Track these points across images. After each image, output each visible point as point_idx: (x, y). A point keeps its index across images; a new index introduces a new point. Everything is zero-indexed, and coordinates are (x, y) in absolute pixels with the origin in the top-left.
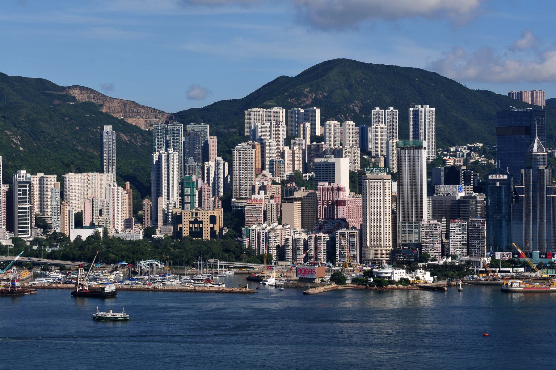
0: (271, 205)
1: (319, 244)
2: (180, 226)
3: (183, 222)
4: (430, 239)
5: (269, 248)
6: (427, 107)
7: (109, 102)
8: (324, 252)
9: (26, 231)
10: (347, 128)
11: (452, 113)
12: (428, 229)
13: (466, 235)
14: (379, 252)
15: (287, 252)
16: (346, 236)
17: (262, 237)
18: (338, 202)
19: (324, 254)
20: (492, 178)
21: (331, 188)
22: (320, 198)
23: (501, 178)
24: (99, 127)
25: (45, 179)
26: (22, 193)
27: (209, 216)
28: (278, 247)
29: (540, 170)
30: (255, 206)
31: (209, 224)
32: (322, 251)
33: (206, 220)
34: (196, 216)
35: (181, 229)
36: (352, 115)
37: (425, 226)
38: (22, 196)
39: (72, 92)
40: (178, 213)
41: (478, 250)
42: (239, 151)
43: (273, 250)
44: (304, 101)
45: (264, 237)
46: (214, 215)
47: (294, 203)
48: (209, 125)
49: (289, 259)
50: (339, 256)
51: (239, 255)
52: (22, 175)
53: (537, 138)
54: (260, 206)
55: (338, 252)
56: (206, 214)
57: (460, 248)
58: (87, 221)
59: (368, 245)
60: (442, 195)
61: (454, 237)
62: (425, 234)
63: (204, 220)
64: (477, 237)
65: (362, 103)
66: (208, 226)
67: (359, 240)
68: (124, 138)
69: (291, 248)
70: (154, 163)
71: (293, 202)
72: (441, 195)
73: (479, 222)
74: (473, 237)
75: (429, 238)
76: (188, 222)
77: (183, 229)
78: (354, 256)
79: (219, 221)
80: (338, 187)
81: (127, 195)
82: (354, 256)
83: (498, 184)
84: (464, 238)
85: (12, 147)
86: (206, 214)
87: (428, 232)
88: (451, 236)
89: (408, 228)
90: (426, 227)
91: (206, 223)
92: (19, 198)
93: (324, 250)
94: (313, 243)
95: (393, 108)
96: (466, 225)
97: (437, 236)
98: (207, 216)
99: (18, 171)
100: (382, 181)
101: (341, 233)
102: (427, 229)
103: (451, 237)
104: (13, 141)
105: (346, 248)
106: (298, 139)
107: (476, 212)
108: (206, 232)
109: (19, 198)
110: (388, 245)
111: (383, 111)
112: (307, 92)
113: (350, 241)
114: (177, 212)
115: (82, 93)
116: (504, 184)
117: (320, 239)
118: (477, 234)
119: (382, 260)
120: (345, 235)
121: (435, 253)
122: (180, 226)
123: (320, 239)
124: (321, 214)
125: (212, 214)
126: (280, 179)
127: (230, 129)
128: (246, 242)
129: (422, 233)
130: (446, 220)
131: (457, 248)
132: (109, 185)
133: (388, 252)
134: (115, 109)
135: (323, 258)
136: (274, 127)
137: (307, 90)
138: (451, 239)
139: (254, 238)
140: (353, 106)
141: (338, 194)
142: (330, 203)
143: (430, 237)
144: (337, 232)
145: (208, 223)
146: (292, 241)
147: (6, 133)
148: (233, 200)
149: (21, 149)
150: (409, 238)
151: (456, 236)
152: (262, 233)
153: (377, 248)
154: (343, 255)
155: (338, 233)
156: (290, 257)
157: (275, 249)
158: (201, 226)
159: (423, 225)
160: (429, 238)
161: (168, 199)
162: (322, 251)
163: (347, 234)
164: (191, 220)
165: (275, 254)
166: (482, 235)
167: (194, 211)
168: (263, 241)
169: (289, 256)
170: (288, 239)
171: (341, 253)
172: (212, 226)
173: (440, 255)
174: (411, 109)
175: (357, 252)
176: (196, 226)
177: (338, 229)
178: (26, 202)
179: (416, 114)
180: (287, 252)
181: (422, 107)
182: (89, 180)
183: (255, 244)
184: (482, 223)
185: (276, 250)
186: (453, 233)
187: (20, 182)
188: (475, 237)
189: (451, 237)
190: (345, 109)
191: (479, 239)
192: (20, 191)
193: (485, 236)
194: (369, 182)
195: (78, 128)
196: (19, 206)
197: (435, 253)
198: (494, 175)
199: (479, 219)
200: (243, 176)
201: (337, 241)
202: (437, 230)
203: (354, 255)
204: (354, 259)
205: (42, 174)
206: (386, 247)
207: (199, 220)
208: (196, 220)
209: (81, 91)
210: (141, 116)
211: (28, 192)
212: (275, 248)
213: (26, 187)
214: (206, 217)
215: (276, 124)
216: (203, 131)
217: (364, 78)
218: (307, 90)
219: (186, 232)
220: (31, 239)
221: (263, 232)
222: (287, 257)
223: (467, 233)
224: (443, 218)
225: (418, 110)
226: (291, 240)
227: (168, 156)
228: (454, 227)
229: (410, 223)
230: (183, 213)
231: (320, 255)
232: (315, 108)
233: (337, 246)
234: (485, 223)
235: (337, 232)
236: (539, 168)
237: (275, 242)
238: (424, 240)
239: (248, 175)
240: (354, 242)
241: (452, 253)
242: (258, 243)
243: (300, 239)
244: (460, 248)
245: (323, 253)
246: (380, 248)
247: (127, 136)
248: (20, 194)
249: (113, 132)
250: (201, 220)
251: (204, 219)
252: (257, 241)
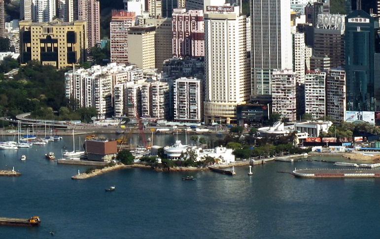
0: (145, 20)
1: (154, 96)
3: (32, 40)
4: (282, 93)
5: (95, 99)
8: (160, 106)
12: (280, 81)
13: (324, 89)
14: (222, 108)
15: (116, 104)
16: (186, 87)
17: (88, 85)
18: (196, 35)
19: (161, 108)
20: (352, 21)
21: (188, 17)
22: (175, 28)
23: (363, 21)
28: (108, 98)
30: (123, 21)
32: (158, 105)
33: (62, 38)
34: (49, 32)
35: (29, 49)
37: (276, 77)
40: (25, 29)
41: (337, 108)
43: (101, 102)
45: (90, 85)
46: (73, 32)
47: (143, 35)
49: (119, 112)
50: (177, 111)
51: (45, 116)
54: (130, 22)
55: (176, 107)
56: (62, 30)
57: (317, 105)
59: (210, 98)
60: (326, 28)
61: (310, 92)
62: (277, 87)
63: (59, 38)
64: (336, 92)
66: (64, 46)
67: (201, 92)
69: (122, 99)
71: (141, 34)
72: (325, 28)
73: (338, 74)
74: (332, 92)
75: (281, 91)
76: (39, 40)
77: (32, 50)
78: (195, 112)
79: (80, 39)
80: (197, 15)
82: (195, 112)
83: (359, 30)
84: (322, 92)
86: (62, 30)
87: (279, 84)
88: (307, 90)
89: (264, 76)
90: (277, 78)
91: (62, 42)
93: (160, 103)
94: (147, 94)
96: (323, 77)
97: (289, 90)
98: (64, 32)
100: (226, 21)
101: (180, 83)
102: (278, 81)
103: (306, 92)
105: (185, 101)
107: (322, 65)
108: (62, 53)
110: (233, 100)
113: (190, 94)
114: (24, 27)
116: (366, 29)
117: (155, 90)
118: (336, 89)
119: (226, 118)
120: (185, 85)
121: (288, 110)
122: (29, 45)
123: (155, 90)
124: (177, 49)
125: (70, 30)
128: (69, 90)
129: (273, 86)
130: (329, 59)
131: (314, 105)
133: (233, 108)
138: (307, 93)
139: (79, 85)
141: (197, 25)
142: (188, 36)
143: (282, 90)
144: (175, 82)
145: (64, 42)
146: (124, 90)
151: (312, 91)
152: (88, 80)
153: (220, 103)
154: (181, 110)
155: (176, 83)
156: (120, 111)
157: (103, 100)
158: (55, 45)
159: (274, 76)
160: (281, 91)
162: (158, 105)
163: (186, 84)
164: (42, 37)
165: (103, 106)
166: (340, 90)
167: (46, 25)
168: (89, 90)
169: (119, 109)
170: (118, 88)
171: (180, 107)
172: (70, 45)
173: (294, 113)
175: (198, 107)
176: (49, 45)
177: (177, 78)
180: (116, 104)
183: (79, 93)
184: (341, 75)
185: (105, 102)
186: (308, 86)
188: (333, 92)
189: (306, 92)
191: (338, 95)
193: (345, 91)
194: (211, 22)
197: (288, 110)
198: (354, 19)
199: (338, 71)
201: (175, 93)
202: (290, 82)
203: (195, 110)
206: (231, 102)
207: (52, 37)
208: (49, 37)
212: (103, 99)
214: (62, 34)
219: (35, 53)
221: (89, 79)
222: (116, 111)
223: (324, 86)
224: (324, 57)
226: (121, 89)
228: (310, 79)
229: (266, 70)
230: (32, 29)
231: (155, 109)
233: (175, 98)
234: (344, 76)
235: (175, 82)
237: (104, 91)
238: (274, 94)
240: (195, 94)
241: (307, 110)
242: (84, 91)
243: (131, 88)
244: (317, 105)
245: (159, 107)
250: (55, 37)
251: (59, 36)
252: (82, 89)
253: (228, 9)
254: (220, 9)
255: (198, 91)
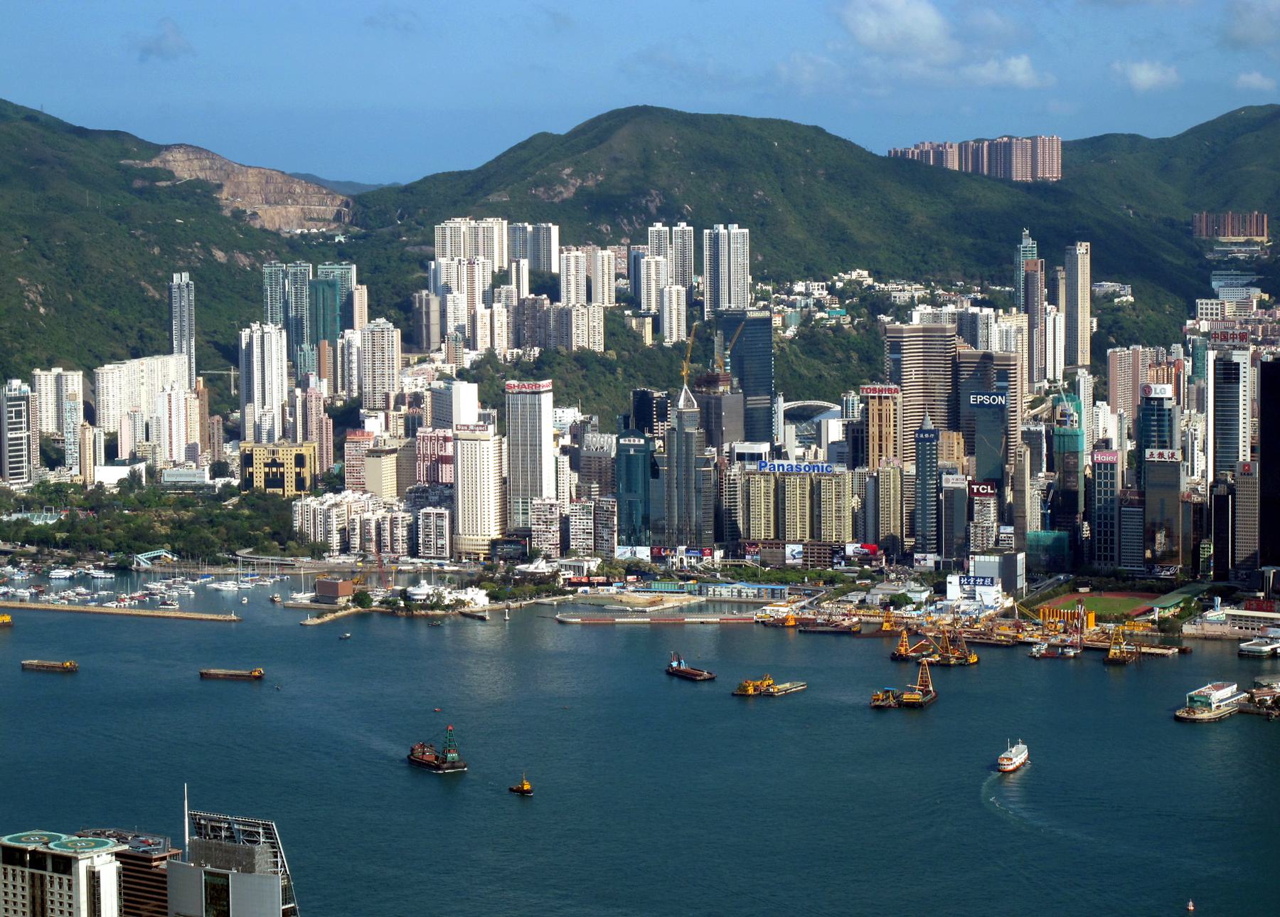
2: (251, 470)
6: (734, 229)
7: (237, 174)
9: (22, 474)
10: (600, 263)
11: (827, 209)
14: (474, 543)
23: (637, 442)
24: (197, 244)
25: (64, 378)
26: (13, 415)
27: (294, 455)
29: (687, 433)
31: (293, 468)
32: (400, 539)
33: (289, 461)
35: (251, 474)
36: (642, 219)
38: (14, 420)
39: (171, 158)
42: (372, 332)
44: (561, 193)
48: (355, 266)
52: (14, 387)
53: (686, 387)
58: (124, 454)
59: (460, 531)
63: (285, 461)
65: (663, 196)
68: (242, 262)
70: (244, 347)
76: (262, 464)
78: (443, 547)
81: (197, 402)
82: (443, 547)
85: (25, 310)
91: (289, 466)
92: (11, 424)
94: (387, 526)
95: (685, 224)
99: (9, 381)
104: (28, 297)
106: (506, 287)
109: (11, 424)
111: (667, 228)
112: (567, 175)
115: (189, 159)
122: (251, 470)
125: (299, 452)
126: (454, 368)
127: (423, 247)
132: (164, 389)
133: (487, 543)
134: (248, 188)
135: (402, 547)
136: (465, 267)
137: (568, 171)
140: (647, 201)
147: (19, 282)
148: (362, 411)
149: (42, 310)
150: (518, 521)
158: (282, 470)
161: (264, 403)
162: (400, 539)
164: (266, 461)
172: (298, 470)
174: (707, 231)
175: (446, 541)
176: (274, 470)
178: (21, 429)
179: (715, 239)
181: (726, 227)
182: (142, 371)
187: (11, 399)
190: (631, 208)
192: (11, 412)
195: (156, 250)
196: (9, 436)
200: (378, 372)
204: (443, 552)
205: (60, 370)
207: (278, 461)
208: (274, 460)
209: (188, 155)
210: (294, 200)
211: (24, 414)
213: (20, 405)
214: (289, 457)
215: (469, 263)
216: (344, 278)
217: (677, 144)
218: (568, 171)
220: (30, 485)
224: (592, 483)
225: (718, 234)
226: (358, 521)
227: (262, 337)
232: (550, 225)
236: (687, 431)
239: (386, 372)
242: (315, 523)
245: (401, 542)
246: (475, 537)
247: (248, 256)
248: (11, 418)
249: (191, 282)
250: (281, 461)
253: (481, 428)
254: (472, 428)
255: (446, 523)
